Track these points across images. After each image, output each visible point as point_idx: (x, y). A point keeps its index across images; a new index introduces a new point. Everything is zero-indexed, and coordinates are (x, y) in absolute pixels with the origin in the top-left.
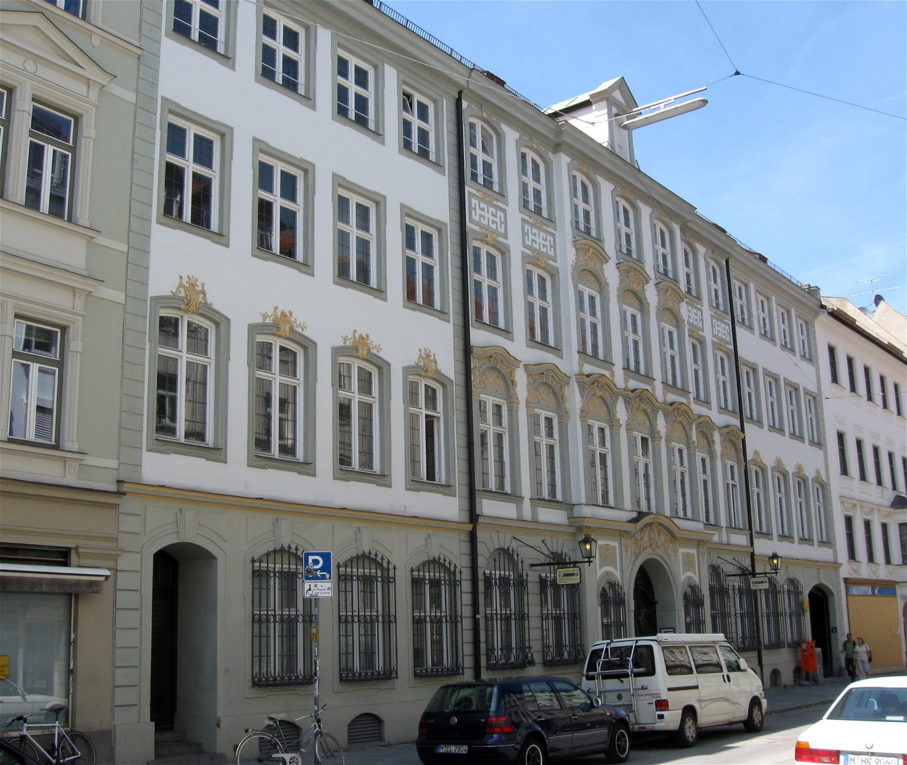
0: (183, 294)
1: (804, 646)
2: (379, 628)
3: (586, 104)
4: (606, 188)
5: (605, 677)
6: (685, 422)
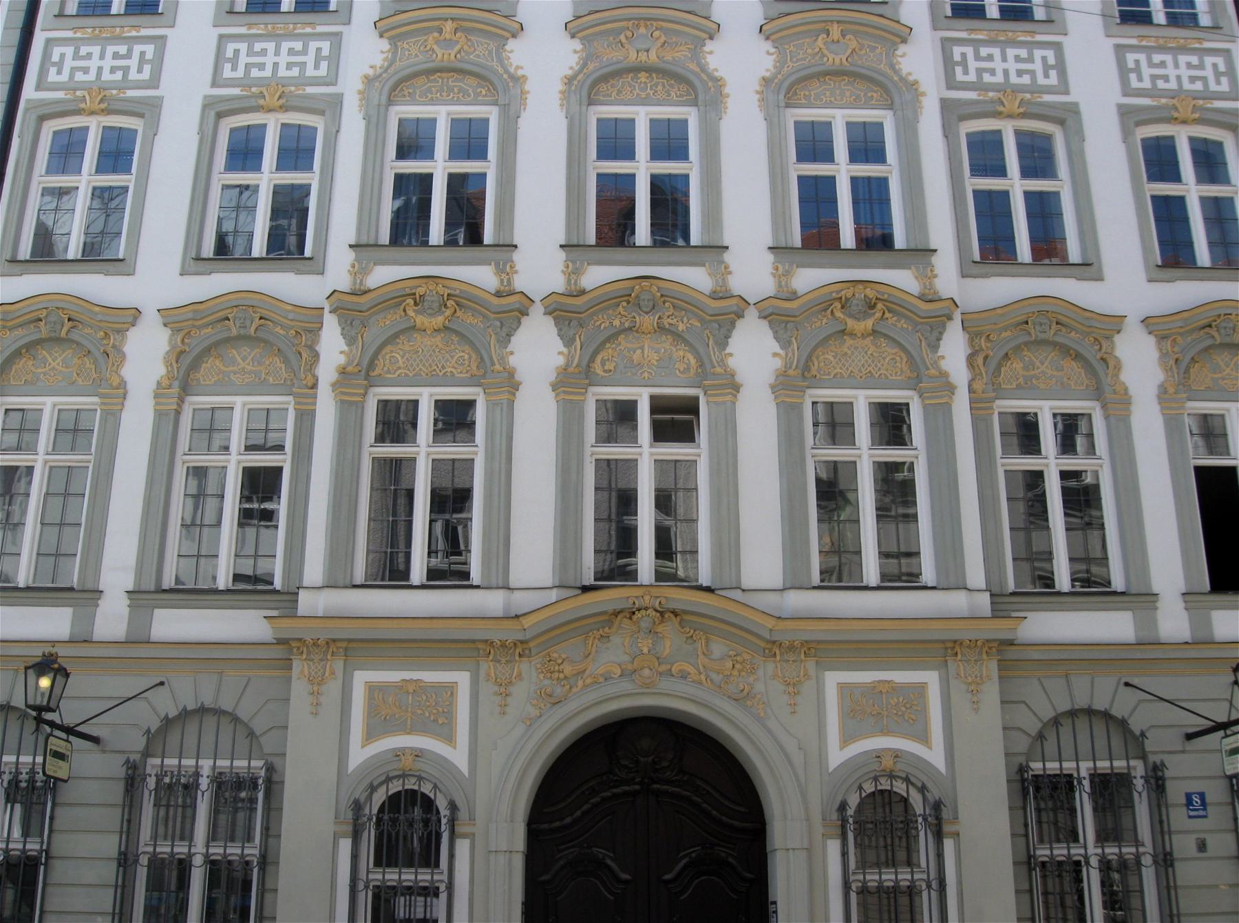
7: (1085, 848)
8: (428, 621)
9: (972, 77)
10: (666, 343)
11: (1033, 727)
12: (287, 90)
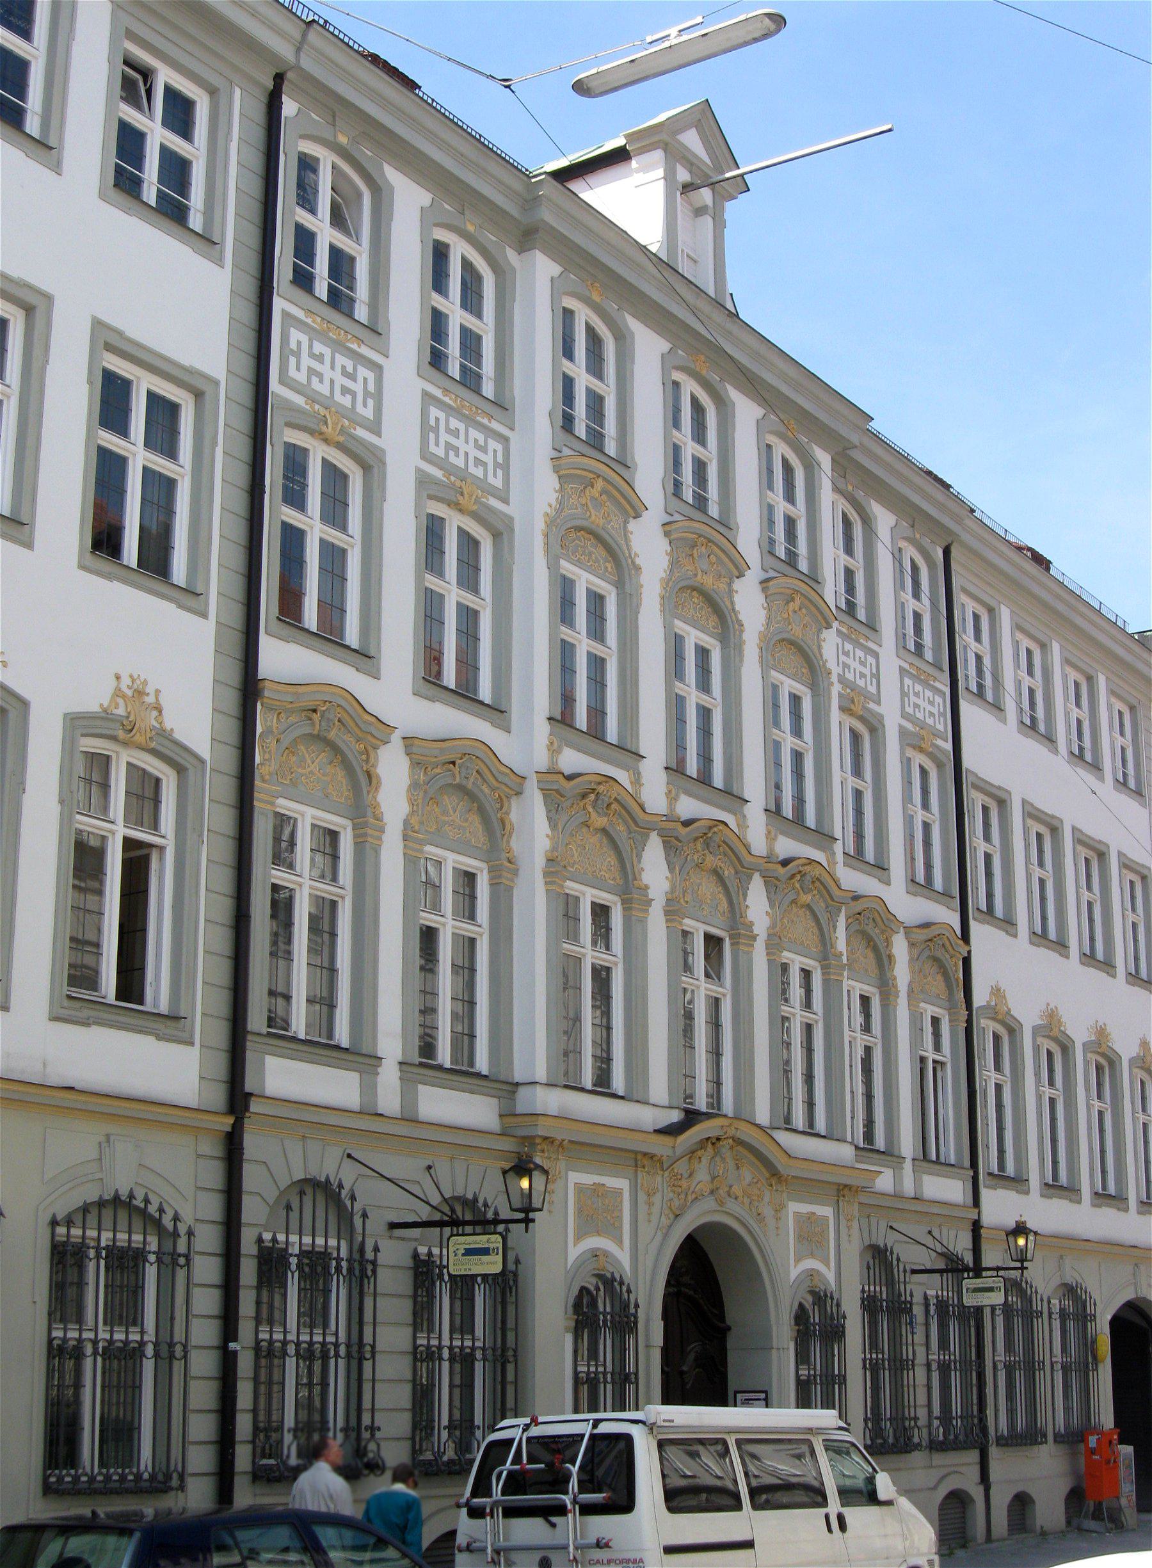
0: (121, 711)
1: (1093, 1441)
2: (338, 1371)
3: (618, 156)
4: (649, 348)
5: (511, 1512)
6: (820, 907)
8: (783, 1154)
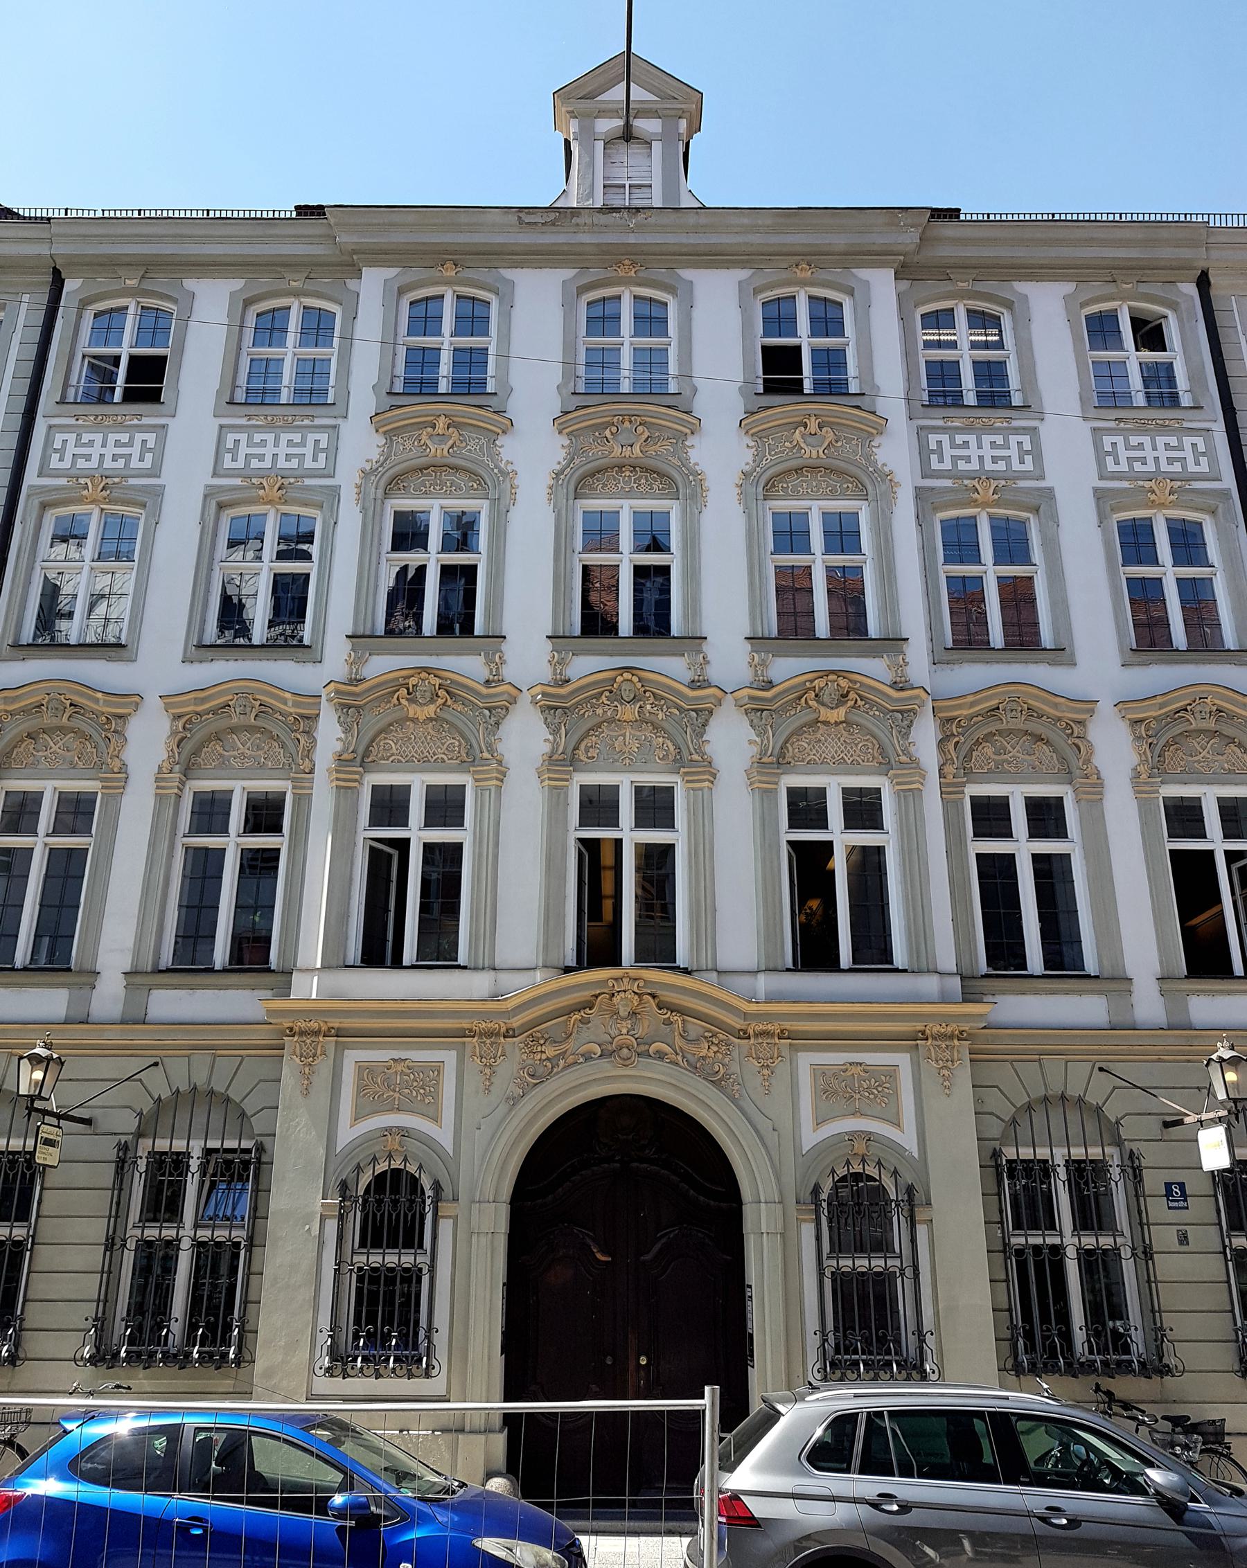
7: (1061, 1236)
9: (948, 465)
10: (647, 732)
11: (1007, 1112)
12: (286, 481)
